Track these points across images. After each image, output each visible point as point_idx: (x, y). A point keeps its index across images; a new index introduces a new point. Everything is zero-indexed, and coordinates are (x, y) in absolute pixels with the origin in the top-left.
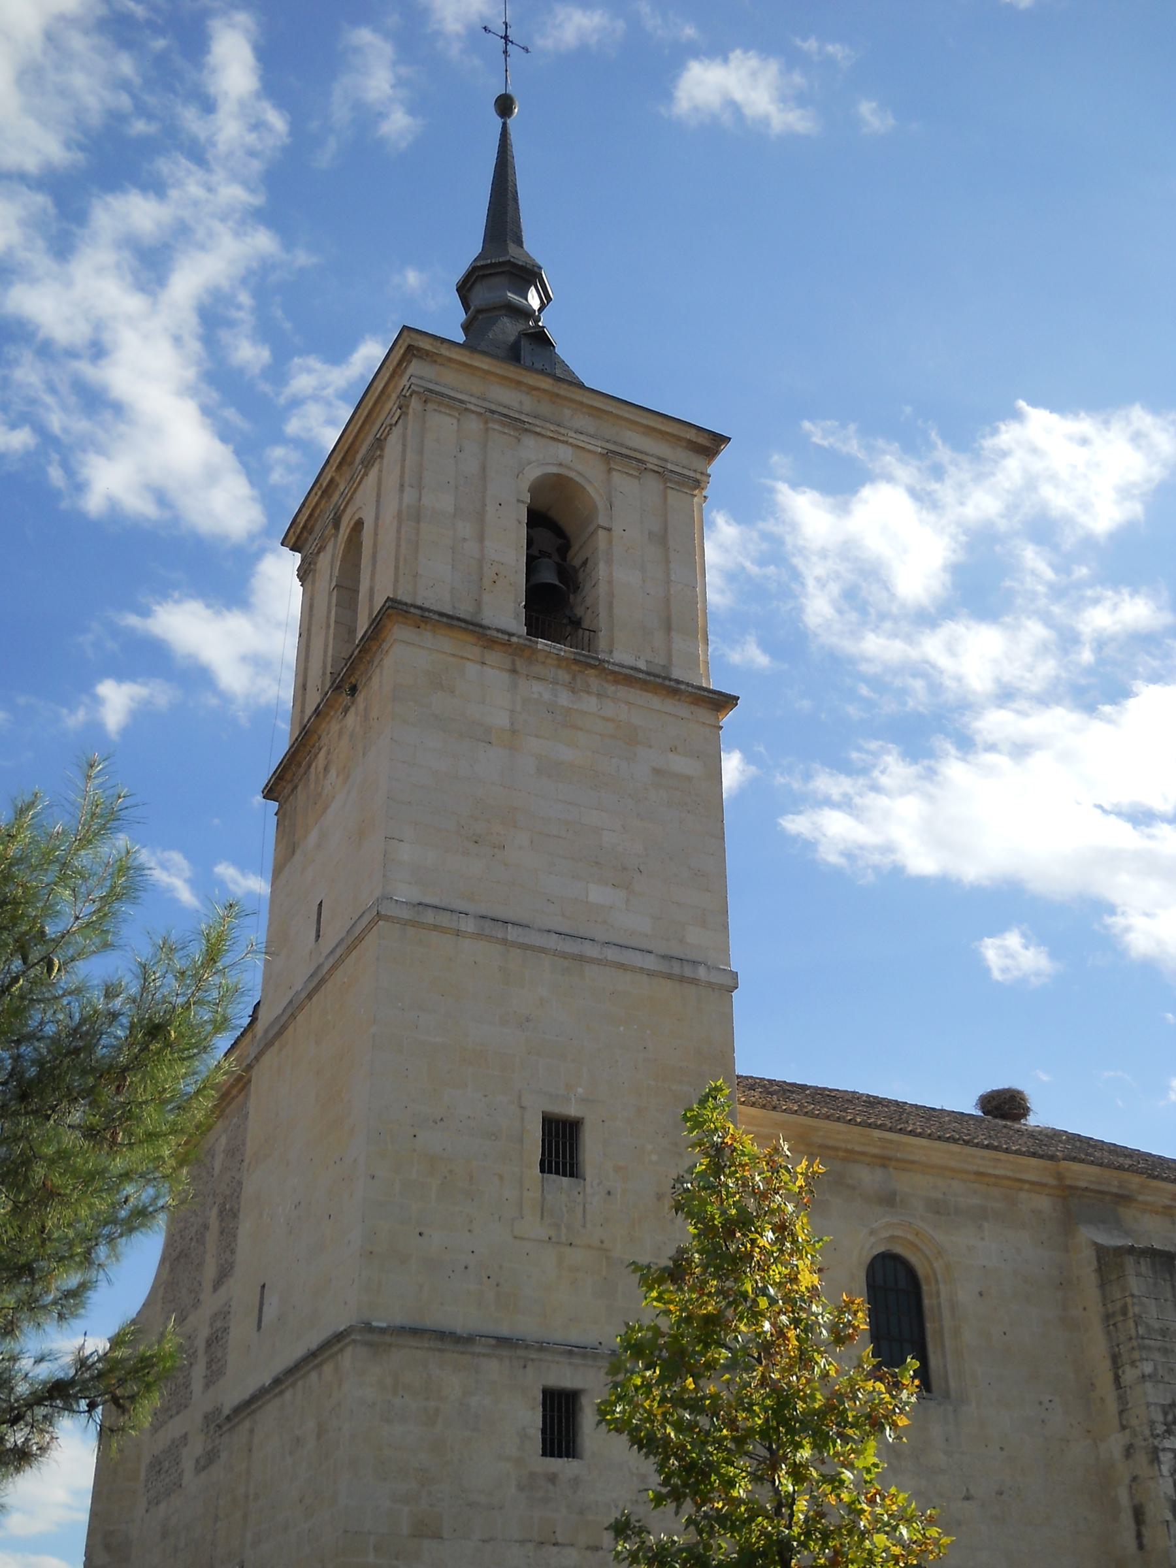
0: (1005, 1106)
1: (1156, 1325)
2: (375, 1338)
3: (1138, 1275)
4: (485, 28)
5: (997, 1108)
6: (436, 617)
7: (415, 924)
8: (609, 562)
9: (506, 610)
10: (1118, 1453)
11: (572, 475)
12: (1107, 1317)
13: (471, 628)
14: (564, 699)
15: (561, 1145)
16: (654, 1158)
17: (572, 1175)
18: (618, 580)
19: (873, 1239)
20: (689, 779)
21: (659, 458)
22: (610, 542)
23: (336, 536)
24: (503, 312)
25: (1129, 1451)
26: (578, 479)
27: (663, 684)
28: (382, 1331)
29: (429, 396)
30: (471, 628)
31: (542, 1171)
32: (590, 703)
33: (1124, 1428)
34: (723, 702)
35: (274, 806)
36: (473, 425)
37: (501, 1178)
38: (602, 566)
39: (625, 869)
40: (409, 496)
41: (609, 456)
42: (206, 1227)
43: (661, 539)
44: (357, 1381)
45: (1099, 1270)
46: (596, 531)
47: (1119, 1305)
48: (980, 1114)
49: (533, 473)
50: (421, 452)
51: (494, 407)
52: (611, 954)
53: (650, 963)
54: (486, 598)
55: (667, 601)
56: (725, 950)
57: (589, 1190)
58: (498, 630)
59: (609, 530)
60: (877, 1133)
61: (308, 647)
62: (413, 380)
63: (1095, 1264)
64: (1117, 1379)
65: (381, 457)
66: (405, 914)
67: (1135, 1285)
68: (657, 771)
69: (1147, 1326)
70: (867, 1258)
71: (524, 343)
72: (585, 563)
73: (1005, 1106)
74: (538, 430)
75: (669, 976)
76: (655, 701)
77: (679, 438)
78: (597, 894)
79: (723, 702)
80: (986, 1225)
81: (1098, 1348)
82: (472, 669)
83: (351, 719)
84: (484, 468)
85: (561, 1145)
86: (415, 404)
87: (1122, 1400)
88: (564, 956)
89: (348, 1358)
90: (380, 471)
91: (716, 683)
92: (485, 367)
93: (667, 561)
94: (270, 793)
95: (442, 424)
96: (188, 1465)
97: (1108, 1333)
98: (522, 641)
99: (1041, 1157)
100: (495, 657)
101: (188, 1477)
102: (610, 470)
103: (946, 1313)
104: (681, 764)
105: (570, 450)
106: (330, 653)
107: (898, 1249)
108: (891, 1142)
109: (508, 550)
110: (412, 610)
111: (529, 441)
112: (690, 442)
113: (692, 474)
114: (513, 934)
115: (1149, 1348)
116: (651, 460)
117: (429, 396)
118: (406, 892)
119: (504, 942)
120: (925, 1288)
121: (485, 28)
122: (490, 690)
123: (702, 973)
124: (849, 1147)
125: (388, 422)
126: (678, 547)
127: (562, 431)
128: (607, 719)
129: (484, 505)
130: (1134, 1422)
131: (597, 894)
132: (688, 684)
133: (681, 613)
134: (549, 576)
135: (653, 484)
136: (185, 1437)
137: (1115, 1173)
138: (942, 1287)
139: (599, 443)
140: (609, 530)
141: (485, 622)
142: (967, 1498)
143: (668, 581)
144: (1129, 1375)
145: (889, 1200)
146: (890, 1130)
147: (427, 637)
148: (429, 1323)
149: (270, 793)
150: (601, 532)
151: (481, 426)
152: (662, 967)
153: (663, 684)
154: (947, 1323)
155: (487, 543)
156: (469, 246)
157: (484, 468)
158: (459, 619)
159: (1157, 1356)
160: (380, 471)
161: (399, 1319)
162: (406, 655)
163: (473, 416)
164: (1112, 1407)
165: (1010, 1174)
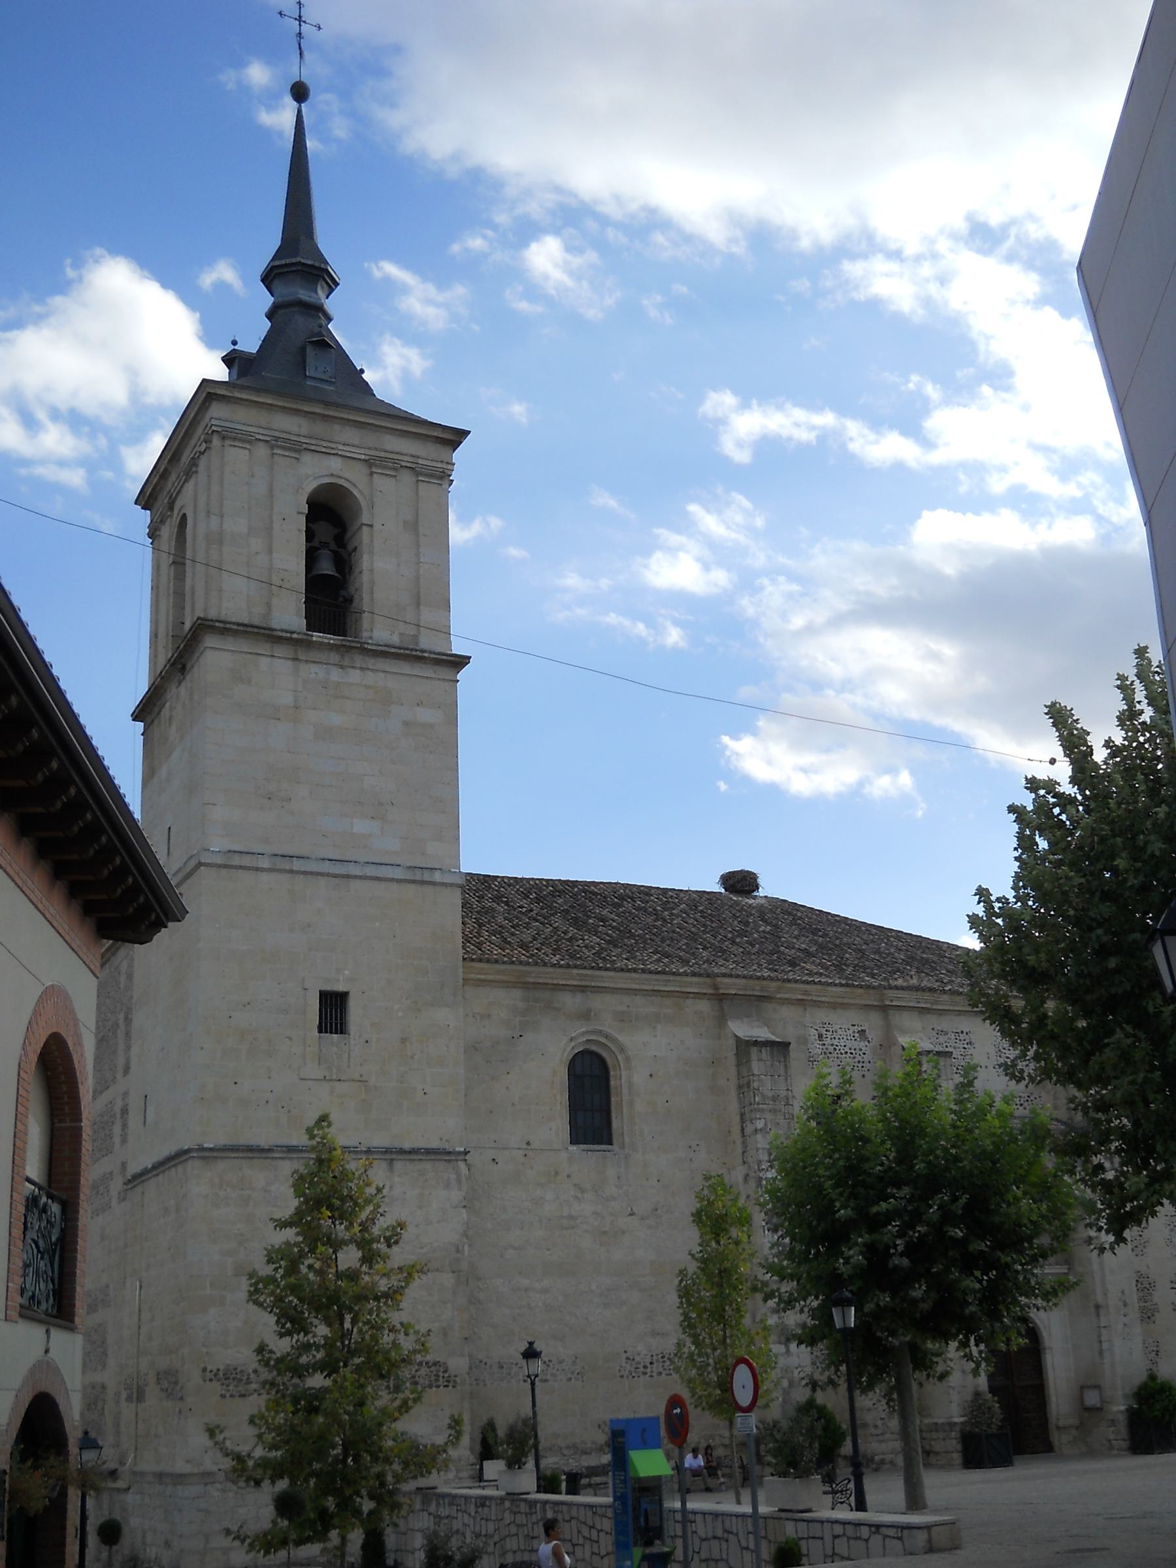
0: (741, 883)
1: (770, 1094)
2: (206, 1154)
3: (760, 1060)
4: (280, 13)
5: (732, 886)
6: (235, 627)
7: (226, 866)
8: (371, 553)
9: (290, 613)
10: (741, 1180)
11: (341, 482)
12: (740, 1087)
13: (262, 634)
14: (335, 675)
15: (333, 1010)
16: (400, 1014)
17: (341, 1033)
18: (379, 568)
19: (573, 1044)
20: (431, 726)
21: (412, 456)
22: (372, 536)
23: (171, 516)
24: (296, 309)
25: (746, 1176)
26: (346, 485)
27: (410, 655)
28: (211, 1149)
29: (226, 435)
30: (262, 634)
31: (320, 1032)
32: (355, 676)
33: (744, 1163)
34: (460, 662)
35: (140, 726)
36: (262, 451)
37: (290, 1039)
38: (365, 557)
39: (381, 804)
40: (214, 521)
41: (369, 463)
42: (117, 1025)
43: (413, 526)
44: (199, 1182)
45: (737, 1054)
46: (360, 528)
47: (746, 1080)
48: (723, 891)
49: (310, 486)
50: (222, 481)
51: (277, 434)
52: (370, 871)
53: (398, 874)
54: (275, 601)
55: (417, 578)
56: (457, 856)
57: (352, 1042)
58: (282, 630)
59: (371, 526)
60: (575, 971)
61: (157, 601)
62: (213, 422)
63: (735, 1052)
64: (743, 1129)
65: (196, 472)
66: (218, 860)
67: (756, 1067)
68: (406, 724)
69: (763, 1095)
70: (567, 1056)
71: (310, 351)
72: (355, 549)
73: (741, 883)
74: (313, 448)
75: (413, 882)
76: (406, 668)
77: (428, 436)
78: (361, 826)
79: (460, 662)
80: (659, 1026)
81: (734, 1107)
82: (264, 662)
83: (183, 690)
84: (271, 490)
85: (333, 1010)
86: (216, 441)
87: (744, 1143)
88: (335, 876)
89: (193, 1167)
90: (196, 484)
91: (458, 648)
92: (270, 401)
93: (418, 546)
94: (137, 716)
95: (236, 456)
96: (114, 1193)
97: (739, 1098)
98: (300, 636)
99: (700, 975)
100: (281, 650)
101: (114, 1202)
102: (372, 474)
103: (625, 1091)
104: (426, 715)
105: (339, 460)
106: (171, 618)
107: (594, 1048)
108: (586, 975)
109: (292, 563)
110: (217, 624)
111: (307, 458)
112: (437, 437)
113: (439, 465)
114: (297, 865)
115: (763, 1110)
116: (406, 458)
117: (226, 435)
118: (218, 844)
119: (291, 871)
120: (612, 1073)
121: (280, 13)
122: (278, 677)
123: (437, 877)
124: (555, 982)
125: (197, 449)
126: (428, 532)
127: (332, 445)
128: (367, 687)
129: (272, 522)
130: (750, 1160)
131: (361, 826)
132: (430, 652)
133: (432, 591)
134: (326, 567)
135: (406, 477)
136: (111, 1173)
137: (757, 982)
138: (623, 1073)
139: (362, 451)
140: (371, 526)
141: (274, 626)
142: (632, 1214)
143: (418, 563)
144: (749, 1129)
145: (586, 1015)
146: (585, 968)
147: (230, 643)
148: (242, 1141)
149: (137, 716)
150: (365, 529)
151: (269, 452)
152: (408, 876)
153: (410, 655)
154: (626, 1098)
155: (275, 555)
156: (267, 241)
157: (271, 490)
158: (252, 626)
159: (768, 1116)
160: (196, 484)
161: (222, 1141)
162: (216, 658)
163: (262, 444)
164: (739, 1150)
165: (677, 989)
